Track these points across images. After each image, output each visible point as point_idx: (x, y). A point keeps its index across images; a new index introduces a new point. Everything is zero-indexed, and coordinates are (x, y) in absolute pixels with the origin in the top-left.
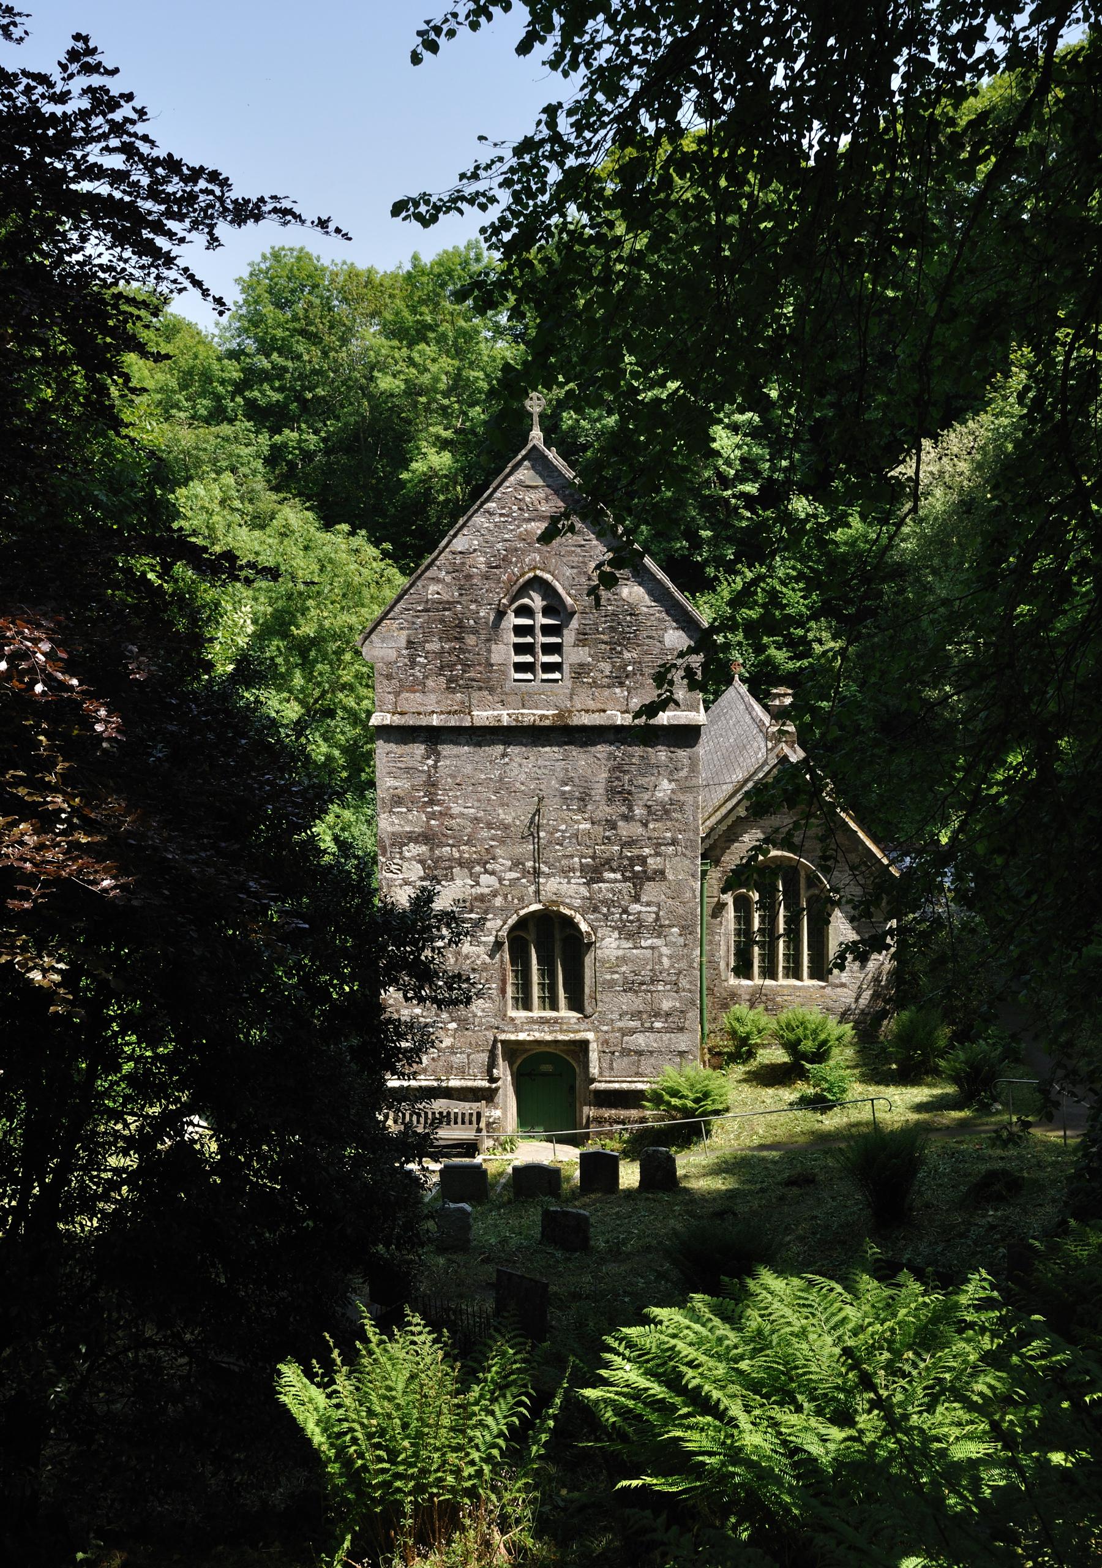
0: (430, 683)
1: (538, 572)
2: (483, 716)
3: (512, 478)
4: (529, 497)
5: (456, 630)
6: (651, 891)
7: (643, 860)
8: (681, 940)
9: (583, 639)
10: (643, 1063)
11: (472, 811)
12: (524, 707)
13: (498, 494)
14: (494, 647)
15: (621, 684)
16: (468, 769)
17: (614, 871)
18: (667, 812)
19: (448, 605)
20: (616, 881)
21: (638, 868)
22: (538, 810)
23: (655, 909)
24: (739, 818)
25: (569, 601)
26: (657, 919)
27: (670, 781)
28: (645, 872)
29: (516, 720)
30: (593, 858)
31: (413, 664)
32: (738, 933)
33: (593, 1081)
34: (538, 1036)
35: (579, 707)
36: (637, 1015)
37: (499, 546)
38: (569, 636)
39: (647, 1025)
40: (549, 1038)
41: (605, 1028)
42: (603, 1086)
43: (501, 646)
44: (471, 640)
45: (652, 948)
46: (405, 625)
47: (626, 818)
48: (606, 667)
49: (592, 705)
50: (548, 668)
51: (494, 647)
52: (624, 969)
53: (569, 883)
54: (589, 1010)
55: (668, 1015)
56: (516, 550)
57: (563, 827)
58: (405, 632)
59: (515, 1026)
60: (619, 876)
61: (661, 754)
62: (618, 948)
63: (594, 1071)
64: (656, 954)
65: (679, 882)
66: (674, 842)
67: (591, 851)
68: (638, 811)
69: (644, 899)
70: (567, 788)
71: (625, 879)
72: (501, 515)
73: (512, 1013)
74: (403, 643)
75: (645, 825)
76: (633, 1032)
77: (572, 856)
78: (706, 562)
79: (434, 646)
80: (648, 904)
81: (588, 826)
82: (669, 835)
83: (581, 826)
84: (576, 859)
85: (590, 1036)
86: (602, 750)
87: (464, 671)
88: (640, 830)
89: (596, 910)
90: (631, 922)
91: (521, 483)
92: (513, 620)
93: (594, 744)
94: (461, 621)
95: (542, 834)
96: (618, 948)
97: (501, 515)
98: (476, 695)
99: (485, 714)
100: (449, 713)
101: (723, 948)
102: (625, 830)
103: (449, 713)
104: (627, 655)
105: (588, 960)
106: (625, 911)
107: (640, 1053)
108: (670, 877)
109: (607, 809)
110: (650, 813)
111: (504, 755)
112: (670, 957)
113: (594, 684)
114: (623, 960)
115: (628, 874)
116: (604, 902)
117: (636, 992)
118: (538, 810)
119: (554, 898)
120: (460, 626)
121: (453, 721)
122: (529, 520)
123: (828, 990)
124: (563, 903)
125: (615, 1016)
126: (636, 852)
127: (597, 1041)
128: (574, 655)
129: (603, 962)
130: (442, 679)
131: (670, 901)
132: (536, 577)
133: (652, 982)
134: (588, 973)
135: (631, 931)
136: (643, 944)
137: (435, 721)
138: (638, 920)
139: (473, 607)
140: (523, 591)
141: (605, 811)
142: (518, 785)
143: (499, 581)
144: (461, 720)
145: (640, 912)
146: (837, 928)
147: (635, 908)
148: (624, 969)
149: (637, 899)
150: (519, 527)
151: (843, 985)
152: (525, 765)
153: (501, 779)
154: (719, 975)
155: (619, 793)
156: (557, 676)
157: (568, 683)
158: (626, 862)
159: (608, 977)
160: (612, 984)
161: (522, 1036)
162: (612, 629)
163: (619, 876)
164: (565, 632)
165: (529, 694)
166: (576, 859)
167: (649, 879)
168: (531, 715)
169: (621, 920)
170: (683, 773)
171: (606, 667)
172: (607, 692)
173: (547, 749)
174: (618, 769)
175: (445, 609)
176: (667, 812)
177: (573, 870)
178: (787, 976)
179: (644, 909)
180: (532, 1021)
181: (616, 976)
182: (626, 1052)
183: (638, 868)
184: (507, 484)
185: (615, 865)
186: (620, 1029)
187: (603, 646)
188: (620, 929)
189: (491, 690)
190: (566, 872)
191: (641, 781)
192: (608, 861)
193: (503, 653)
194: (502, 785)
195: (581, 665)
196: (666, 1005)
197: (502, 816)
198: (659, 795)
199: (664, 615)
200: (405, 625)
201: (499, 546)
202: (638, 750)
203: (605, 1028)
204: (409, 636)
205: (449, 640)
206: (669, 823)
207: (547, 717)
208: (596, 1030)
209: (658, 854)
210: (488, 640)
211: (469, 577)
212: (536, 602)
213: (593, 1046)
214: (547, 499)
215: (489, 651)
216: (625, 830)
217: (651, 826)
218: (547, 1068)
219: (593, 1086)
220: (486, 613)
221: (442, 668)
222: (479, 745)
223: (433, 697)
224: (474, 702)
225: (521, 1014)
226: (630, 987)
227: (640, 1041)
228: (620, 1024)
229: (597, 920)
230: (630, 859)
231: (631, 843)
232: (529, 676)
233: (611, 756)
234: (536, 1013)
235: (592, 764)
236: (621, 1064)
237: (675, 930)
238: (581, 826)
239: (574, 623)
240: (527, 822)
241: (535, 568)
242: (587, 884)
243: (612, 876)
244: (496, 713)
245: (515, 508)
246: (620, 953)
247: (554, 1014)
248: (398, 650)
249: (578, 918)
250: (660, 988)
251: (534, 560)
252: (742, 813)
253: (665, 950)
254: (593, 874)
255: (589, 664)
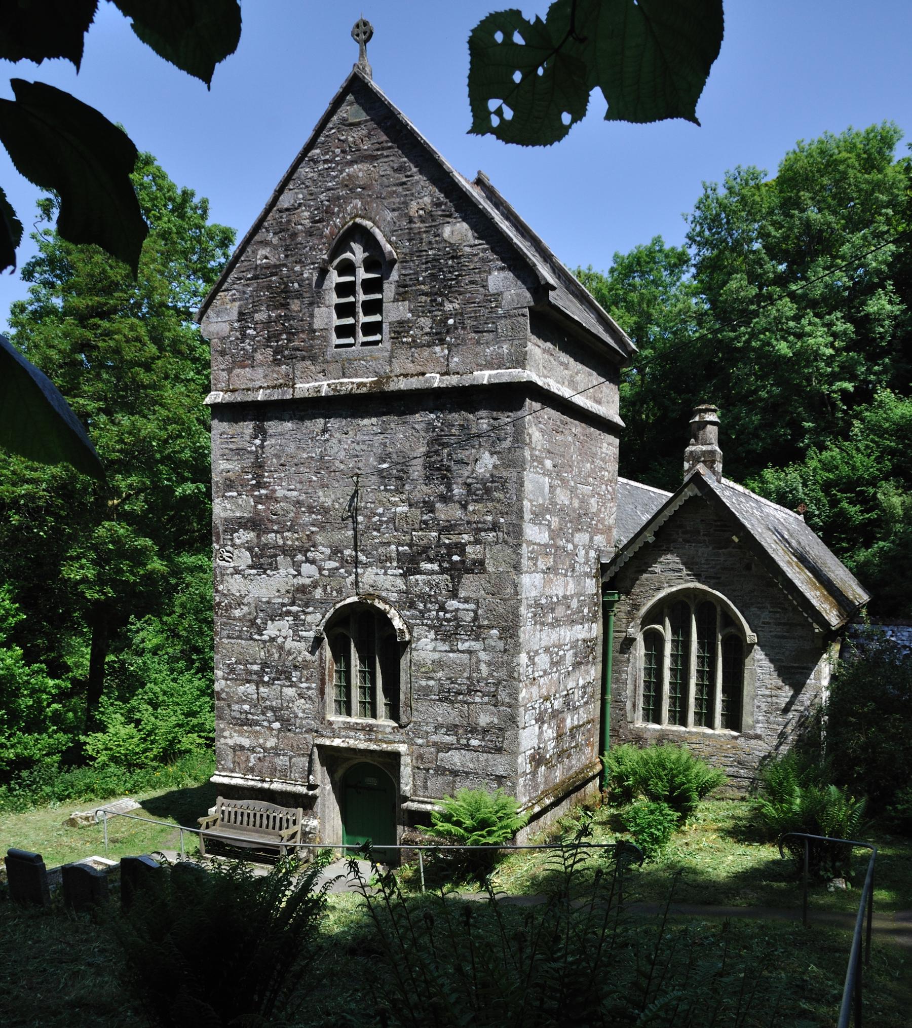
0: (258, 356)
1: (358, 220)
2: (304, 388)
3: (335, 118)
4: (352, 136)
5: (281, 297)
6: (470, 585)
7: (460, 548)
8: (501, 645)
9: (401, 296)
10: (458, 784)
11: (295, 493)
12: (344, 376)
13: (322, 139)
14: (316, 310)
15: (442, 342)
16: (291, 448)
17: (431, 561)
18: (488, 491)
19: (274, 269)
20: (432, 572)
21: (456, 558)
22: (356, 492)
23: (472, 606)
24: (646, 543)
25: (388, 247)
26: (476, 618)
27: (492, 454)
28: (463, 562)
29: (335, 390)
30: (410, 545)
31: (244, 336)
32: (648, 671)
33: (406, 799)
34: (352, 743)
35: (398, 371)
36: (452, 729)
37: (323, 197)
38: (389, 290)
39: (464, 741)
40: (362, 745)
41: (420, 741)
42: (414, 806)
43: (323, 309)
44: (295, 305)
45: (470, 652)
46: (238, 295)
47: (445, 499)
48: (426, 322)
49: (411, 368)
50: (370, 329)
51: (316, 310)
52: (440, 675)
53: (385, 574)
54: (404, 719)
55: (485, 731)
56: (339, 198)
57: (380, 510)
58: (237, 304)
59: (333, 730)
60: (436, 567)
61: (482, 421)
62: (434, 650)
63: (406, 787)
64: (474, 660)
65: (499, 575)
66: (495, 527)
67: (408, 537)
68: (457, 491)
69: (462, 594)
70: (385, 466)
71: (443, 571)
72: (326, 161)
73: (332, 717)
74: (234, 315)
75: (464, 507)
76: (448, 748)
77: (389, 544)
78: (808, 446)
79: (260, 316)
80: (466, 600)
81: (406, 509)
82: (489, 518)
83: (399, 509)
84: (393, 547)
85: (403, 748)
86: (420, 419)
87: (289, 340)
88: (459, 513)
89: (412, 605)
90: (448, 620)
91: (344, 122)
92: (334, 278)
93: (413, 413)
94: (287, 286)
95: (360, 519)
96: (434, 650)
97: (326, 161)
98: (300, 365)
99: (307, 386)
100: (274, 387)
101: (630, 687)
102: (445, 513)
103: (274, 387)
104: (448, 307)
105: (404, 662)
106: (442, 608)
107: (455, 773)
108: (490, 569)
109: (424, 488)
110: (470, 492)
111: (325, 431)
112: (489, 664)
113: (414, 344)
114: (439, 664)
115: (445, 565)
116: (421, 596)
117: (452, 702)
118: (356, 492)
119: (371, 591)
120: (286, 291)
121: (276, 395)
122: (351, 163)
123: (741, 742)
124: (379, 597)
125: (430, 729)
126: (455, 539)
127: (411, 754)
128: (395, 311)
129: (419, 665)
130: (270, 351)
131: (489, 597)
132: (355, 224)
133: (469, 692)
134: (404, 677)
135: (448, 632)
136: (461, 646)
137: (260, 396)
138: (456, 618)
139: (297, 268)
140: (342, 245)
141: (422, 491)
142: (337, 463)
143: (321, 236)
144: (284, 393)
145: (457, 610)
146: (753, 673)
147: (453, 604)
148: (440, 675)
149: (454, 595)
150: (341, 172)
151: (758, 737)
152: (351, 442)
153: (322, 458)
154: (624, 715)
155: (439, 471)
156: (377, 337)
157: (387, 345)
158: (443, 551)
159: (424, 683)
160: (427, 691)
161: (337, 742)
162: (433, 277)
163: (436, 567)
164: (385, 286)
165: (349, 360)
166: (393, 547)
167: (470, 571)
168: (349, 383)
169: (438, 618)
170: (507, 444)
171: (426, 322)
172: (426, 352)
173: (366, 421)
174: (437, 442)
175: (273, 274)
176: (488, 491)
177: (390, 559)
178: (698, 723)
179: (461, 606)
180: (350, 727)
181: (432, 683)
182: (441, 771)
183: (456, 558)
184: (330, 125)
185: (432, 553)
186: (435, 744)
187: (424, 298)
188: (437, 629)
189: (313, 359)
190: (382, 562)
191: (461, 455)
192: (426, 549)
193: (326, 317)
194: (323, 464)
195: (401, 323)
196: (484, 720)
197: (322, 499)
198: (480, 470)
199: (490, 255)
200: (238, 295)
201: (323, 197)
202: (456, 418)
203: (420, 741)
204: (240, 307)
205: (276, 308)
206: (490, 504)
207: (364, 384)
208: (411, 743)
209: (477, 542)
210: (311, 304)
211: (294, 235)
212: (357, 254)
213: (405, 760)
214: (369, 136)
215: (312, 316)
216: (445, 513)
217: (471, 508)
218: (372, 781)
219: (405, 805)
220: (310, 274)
221: (269, 339)
222: (302, 419)
223: (260, 371)
224: (298, 373)
225: (339, 719)
226: (445, 696)
227: (456, 759)
228: (434, 738)
229: (414, 617)
230: (448, 547)
231: (449, 528)
232: (351, 340)
233: (430, 427)
234: (353, 720)
235: (409, 435)
236: (436, 783)
237: (494, 632)
238: (399, 509)
239: (395, 276)
240: (346, 504)
241: (356, 216)
242: (404, 575)
243: (429, 566)
244: (317, 384)
245: (338, 151)
246: (436, 656)
247: (371, 721)
248: (231, 323)
249: (393, 613)
250: (478, 699)
251: (355, 207)
252: (651, 539)
253: (483, 656)
254: (410, 564)
255: (408, 321)
